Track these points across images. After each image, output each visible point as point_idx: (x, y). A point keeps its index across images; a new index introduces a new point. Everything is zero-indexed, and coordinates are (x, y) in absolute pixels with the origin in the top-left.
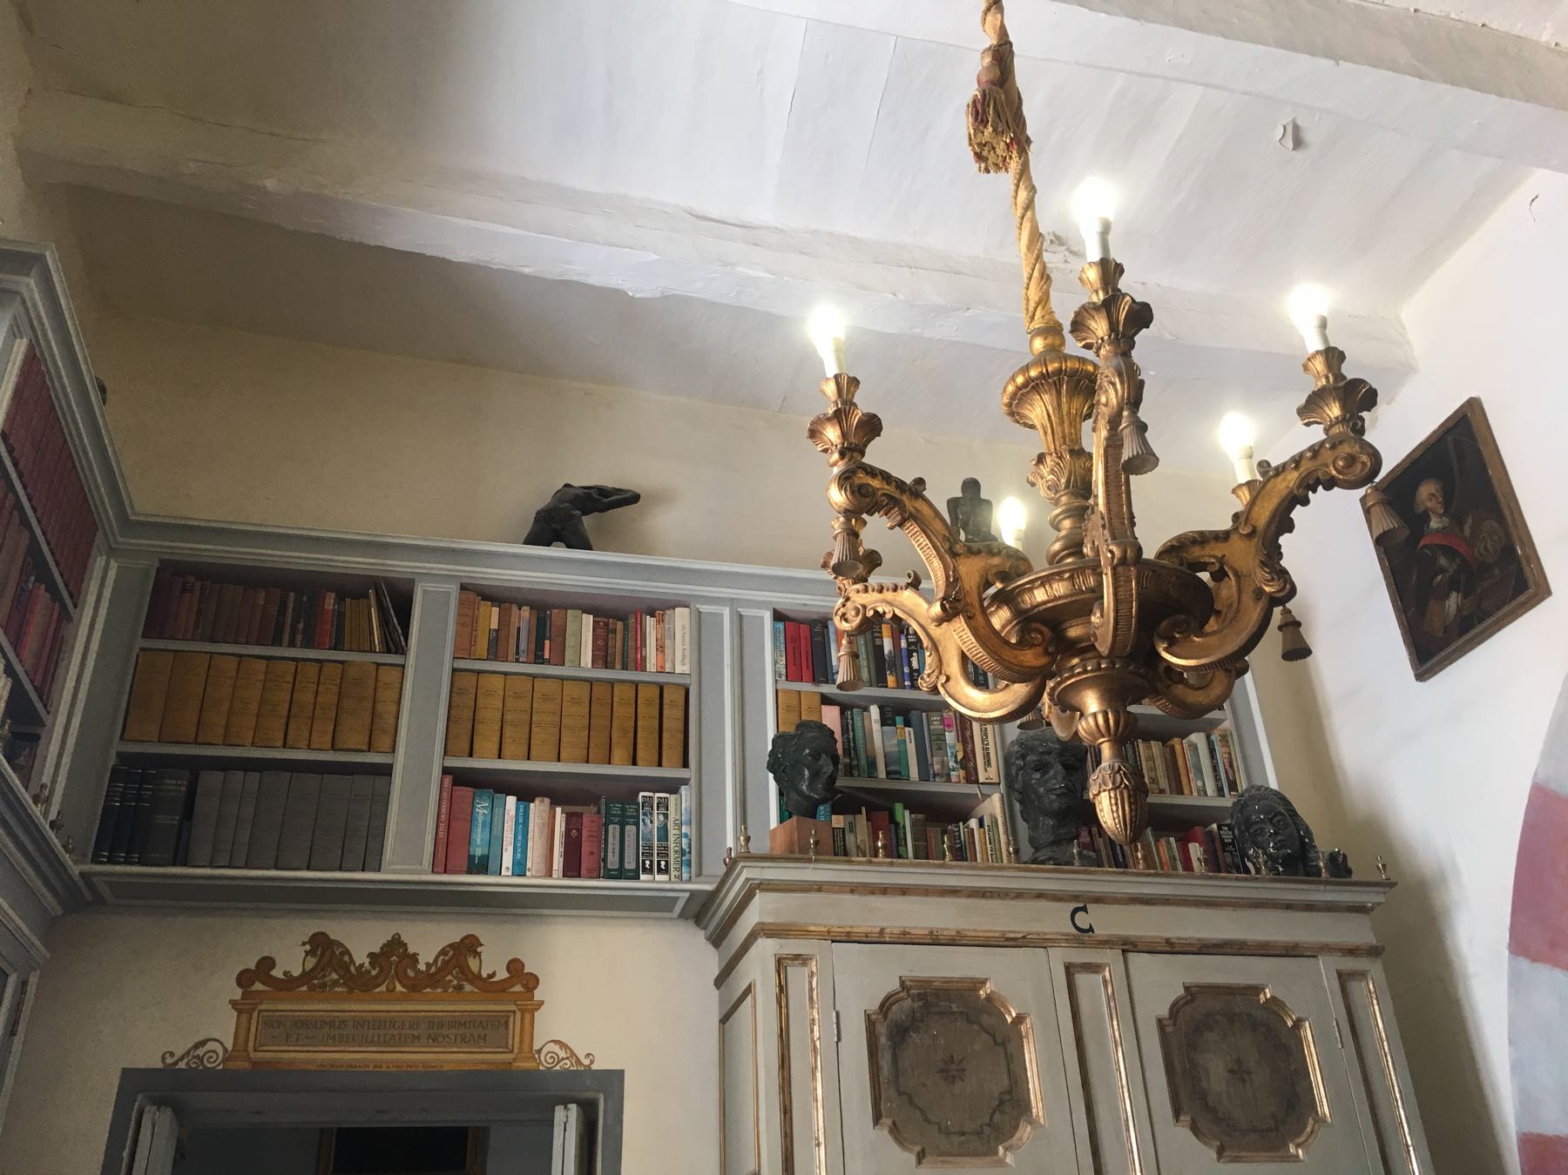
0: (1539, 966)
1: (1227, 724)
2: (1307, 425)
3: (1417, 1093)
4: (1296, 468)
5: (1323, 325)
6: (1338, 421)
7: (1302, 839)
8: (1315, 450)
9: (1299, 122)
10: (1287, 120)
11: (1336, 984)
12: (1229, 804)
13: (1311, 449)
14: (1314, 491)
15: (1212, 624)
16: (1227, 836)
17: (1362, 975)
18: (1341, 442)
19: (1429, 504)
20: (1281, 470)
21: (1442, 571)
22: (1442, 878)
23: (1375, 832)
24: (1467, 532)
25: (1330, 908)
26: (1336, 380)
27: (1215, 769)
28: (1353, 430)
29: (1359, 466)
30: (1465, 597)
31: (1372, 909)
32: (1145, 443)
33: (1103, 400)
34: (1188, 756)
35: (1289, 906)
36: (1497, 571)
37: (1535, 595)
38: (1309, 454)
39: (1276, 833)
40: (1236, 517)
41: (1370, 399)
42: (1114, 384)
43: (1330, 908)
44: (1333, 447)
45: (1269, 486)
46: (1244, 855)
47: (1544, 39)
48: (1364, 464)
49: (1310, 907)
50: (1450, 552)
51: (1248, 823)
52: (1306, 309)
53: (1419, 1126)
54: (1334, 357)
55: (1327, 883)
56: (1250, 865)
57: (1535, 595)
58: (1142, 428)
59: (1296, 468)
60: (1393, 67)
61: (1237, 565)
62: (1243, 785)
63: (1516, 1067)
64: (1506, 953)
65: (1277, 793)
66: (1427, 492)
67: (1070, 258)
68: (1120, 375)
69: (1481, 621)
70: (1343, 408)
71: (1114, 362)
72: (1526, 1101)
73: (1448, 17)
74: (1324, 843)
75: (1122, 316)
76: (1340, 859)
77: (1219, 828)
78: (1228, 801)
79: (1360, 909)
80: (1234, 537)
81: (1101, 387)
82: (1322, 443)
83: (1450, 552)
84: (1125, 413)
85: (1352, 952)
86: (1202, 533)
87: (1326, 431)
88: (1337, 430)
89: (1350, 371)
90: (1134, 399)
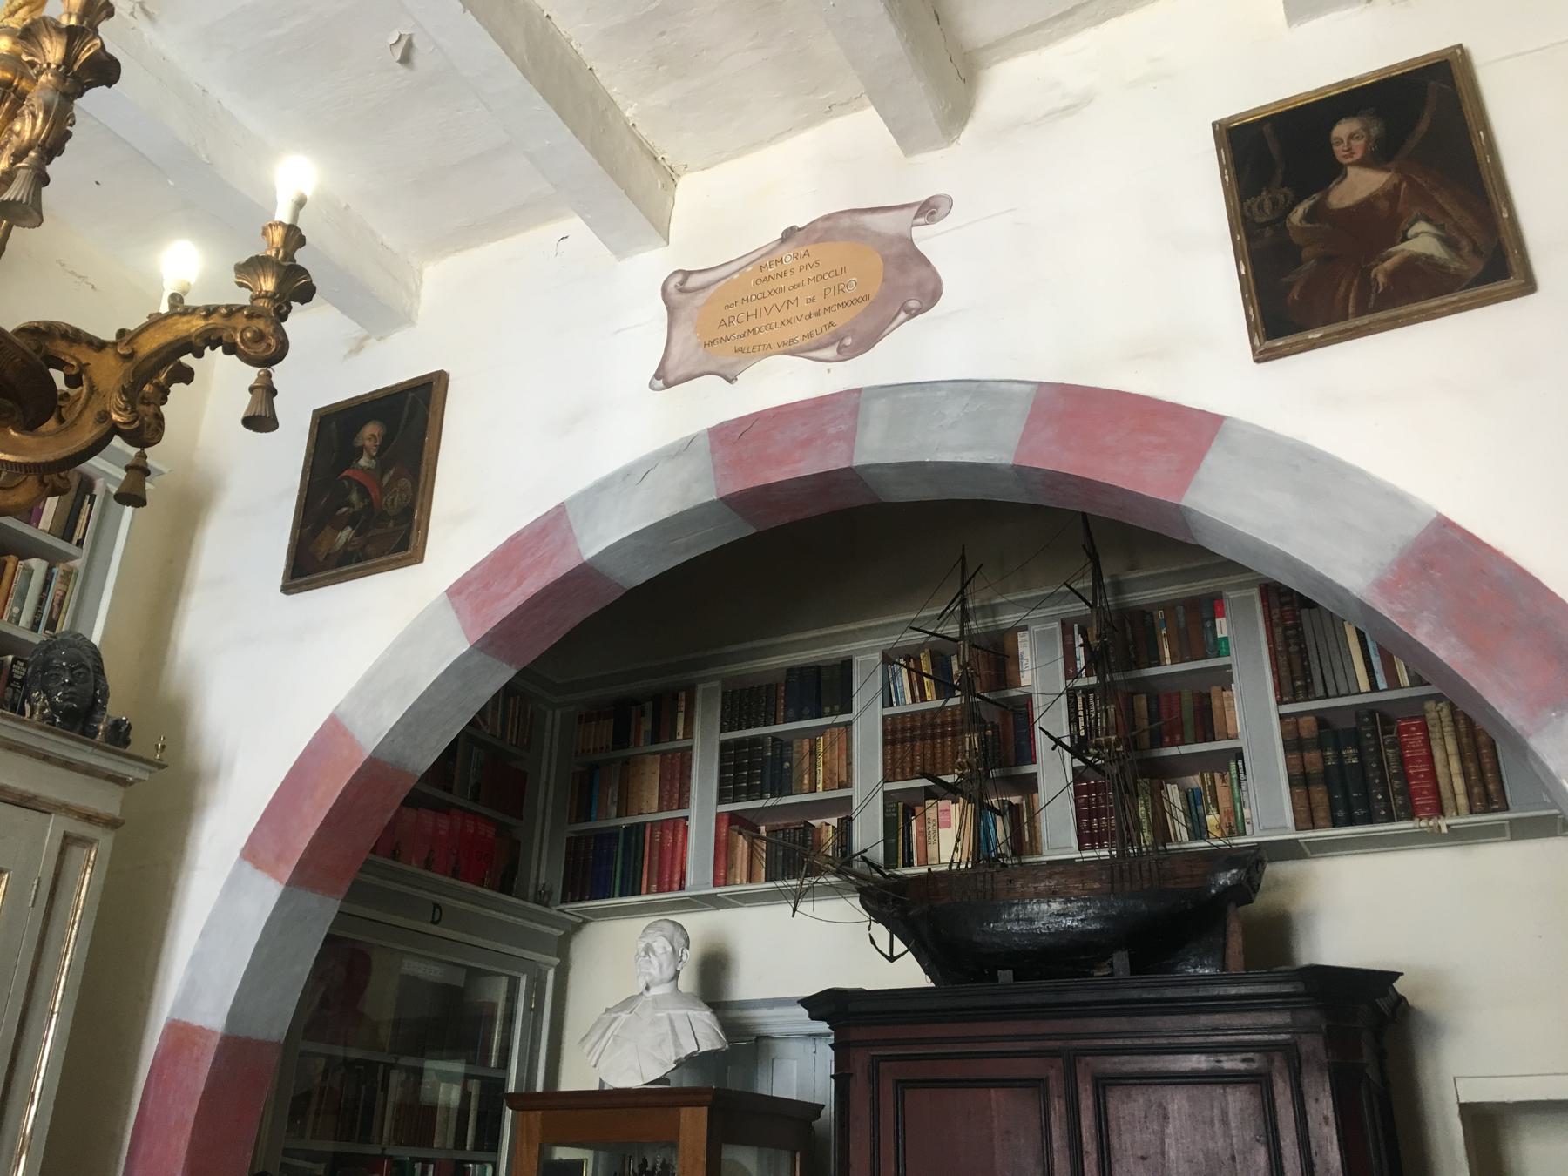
0: (258, 873)
1: (78, 564)
2: (241, 285)
3: (85, 970)
4: (206, 317)
5: (300, 204)
6: (266, 296)
7: (95, 698)
8: (232, 311)
9: (415, 41)
10: (406, 32)
11: (57, 843)
12: (37, 641)
13: (227, 307)
14: (213, 349)
15: (51, 424)
16: (19, 672)
17: (87, 842)
18: (259, 316)
19: (367, 443)
20: (190, 312)
21: (349, 504)
22: (215, 775)
23: (174, 718)
24: (386, 480)
25: (90, 771)
26: (285, 258)
27: (41, 601)
28: (277, 311)
29: (264, 346)
30: (356, 535)
31: (131, 783)
32: (37, 196)
33: (17, 127)
34: (18, 577)
35: (46, 758)
36: (391, 523)
37: (410, 557)
38: (224, 311)
39: (70, 684)
40: (122, 333)
41: (306, 293)
42: (35, 117)
43: (90, 771)
44: (250, 317)
45: (170, 321)
46: (27, 696)
47: (627, 114)
48: (269, 346)
49: (68, 765)
50: (364, 492)
51: (46, 665)
52: (294, 179)
53: (74, 997)
54: (294, 237)
55: (97, 746)
56: (27, 707)
57: (410, 557)
58: (43, 180)
59: (206, 317)
60: (507, 49)
61: (96, 379)
62: (64, 626)
63: (196, 960)
64: (238, 854)
65: (95, 652)
66: (371, 432)
67: (139, 13)
68: (47, 112)
69: (359, 561)
70: (279, 286)
71: (49, 96)
72: (191, 989)
73: (569, 41)
74: (115, 708)
75: (84, 56)
76: (123, 728)
77: (15, 661)
78: (36, 639)
79: (120, 781)
80: (110, 351)
81: (22, 115)
82: (243, 307)
83: (364, 492)
84: (32, 154)
85: (89, 818)
86: (77, 331)
87: (253, 299)
88: (262, 303)
89: (301, 258)
90: (53, 146)
